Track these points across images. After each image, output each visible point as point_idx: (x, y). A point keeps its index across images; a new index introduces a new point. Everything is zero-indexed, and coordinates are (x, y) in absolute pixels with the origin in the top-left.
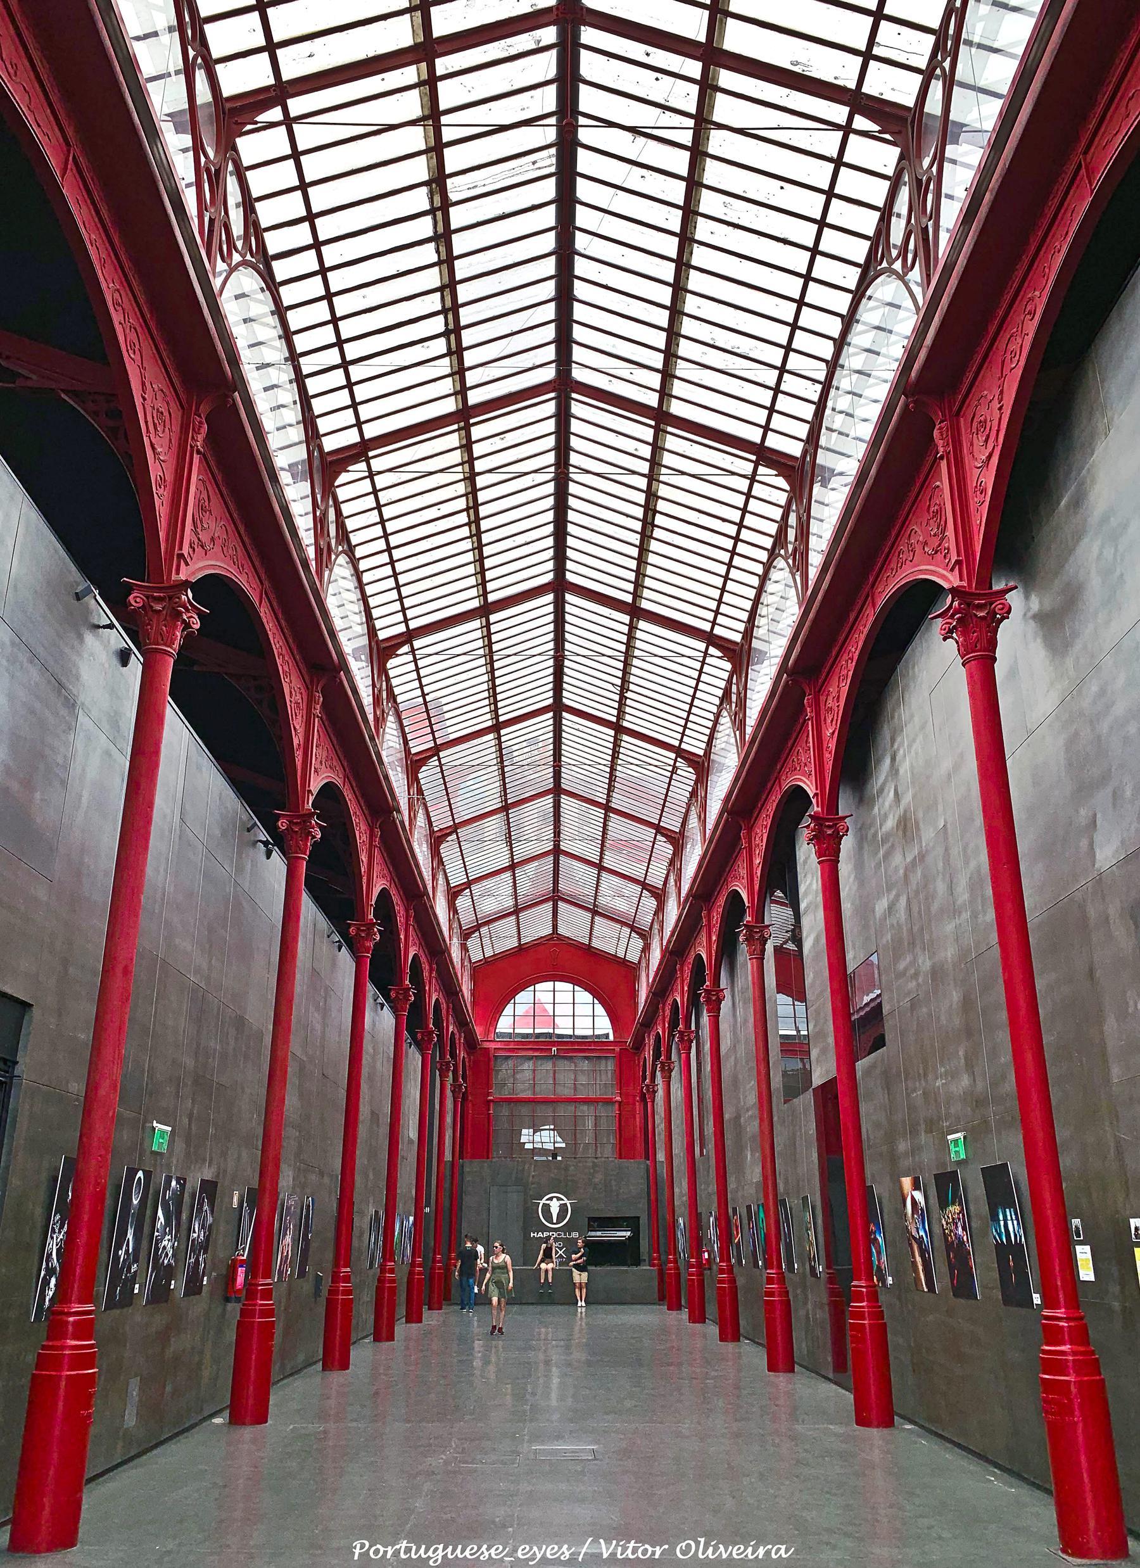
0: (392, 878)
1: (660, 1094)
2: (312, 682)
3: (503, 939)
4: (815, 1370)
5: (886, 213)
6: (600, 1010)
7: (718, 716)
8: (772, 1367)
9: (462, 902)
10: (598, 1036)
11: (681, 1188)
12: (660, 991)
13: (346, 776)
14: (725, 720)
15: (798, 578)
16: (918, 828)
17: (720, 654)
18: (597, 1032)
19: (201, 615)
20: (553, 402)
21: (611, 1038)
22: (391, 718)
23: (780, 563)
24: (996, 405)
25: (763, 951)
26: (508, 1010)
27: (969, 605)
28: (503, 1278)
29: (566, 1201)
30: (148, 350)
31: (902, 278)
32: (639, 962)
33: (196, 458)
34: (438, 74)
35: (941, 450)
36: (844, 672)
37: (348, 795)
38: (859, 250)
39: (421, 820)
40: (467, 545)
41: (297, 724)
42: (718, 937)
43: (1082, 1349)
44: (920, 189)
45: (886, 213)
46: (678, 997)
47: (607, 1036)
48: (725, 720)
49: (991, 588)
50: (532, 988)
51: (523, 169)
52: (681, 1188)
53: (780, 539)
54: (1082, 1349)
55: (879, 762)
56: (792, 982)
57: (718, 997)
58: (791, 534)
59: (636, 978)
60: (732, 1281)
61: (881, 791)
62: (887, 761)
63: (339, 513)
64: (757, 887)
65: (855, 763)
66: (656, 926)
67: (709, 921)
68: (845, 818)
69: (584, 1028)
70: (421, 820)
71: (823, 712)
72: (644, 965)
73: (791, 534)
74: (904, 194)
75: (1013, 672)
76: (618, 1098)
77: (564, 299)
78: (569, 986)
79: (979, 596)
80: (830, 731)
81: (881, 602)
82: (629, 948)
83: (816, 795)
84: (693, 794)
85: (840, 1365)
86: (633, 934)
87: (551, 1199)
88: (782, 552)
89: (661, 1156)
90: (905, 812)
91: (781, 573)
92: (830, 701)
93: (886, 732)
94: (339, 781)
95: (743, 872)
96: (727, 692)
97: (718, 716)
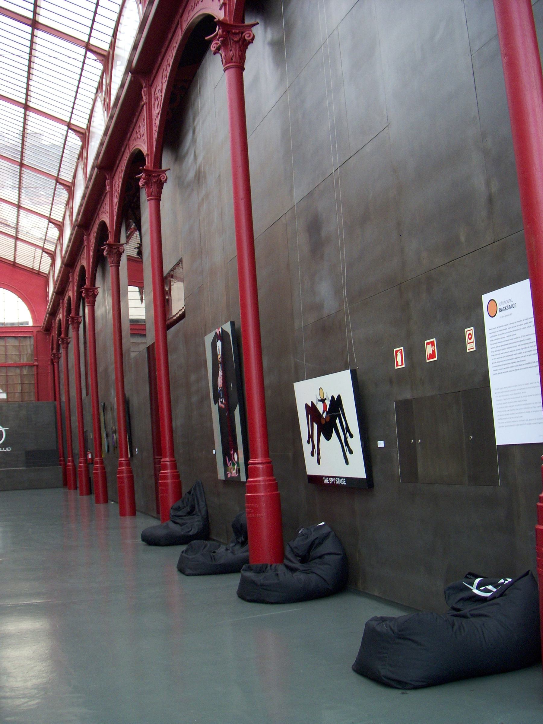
1: (62, 361)
4: (146, 513)
7: (95, 101)
8: (122, 513)
11: (75, 418)
12: (60, 292)
16: (205, 177)
17: (95, 58)
25: (119, 261)
27: (228, 32)
36: (165, 73)
42: (94, 253)
43: (271, 478)
46: (71, 293)
47: (27, 323)
49: (243, 22)
52: (75, 418)
54: (271, 478)
55: (186, 134)
56: (136, 280)
57: (119, 251)
59: (47, 284)
61: (187, 153)
65: (174, 131)
67: (88, 243)
68: (123, 244)
71: (153, 100)
72: (51, 274)
75: (256, 79)
76: (36, 363)
80: (157, 111)
81: (185, 26)
82: (44, 265)
85: (158, 513)
86: (44, 254)
89: (64, 398)
90: (200, 166)
93: (191, 114)
95: (107, 208)
96: (100, 84)
97: (95, 101)
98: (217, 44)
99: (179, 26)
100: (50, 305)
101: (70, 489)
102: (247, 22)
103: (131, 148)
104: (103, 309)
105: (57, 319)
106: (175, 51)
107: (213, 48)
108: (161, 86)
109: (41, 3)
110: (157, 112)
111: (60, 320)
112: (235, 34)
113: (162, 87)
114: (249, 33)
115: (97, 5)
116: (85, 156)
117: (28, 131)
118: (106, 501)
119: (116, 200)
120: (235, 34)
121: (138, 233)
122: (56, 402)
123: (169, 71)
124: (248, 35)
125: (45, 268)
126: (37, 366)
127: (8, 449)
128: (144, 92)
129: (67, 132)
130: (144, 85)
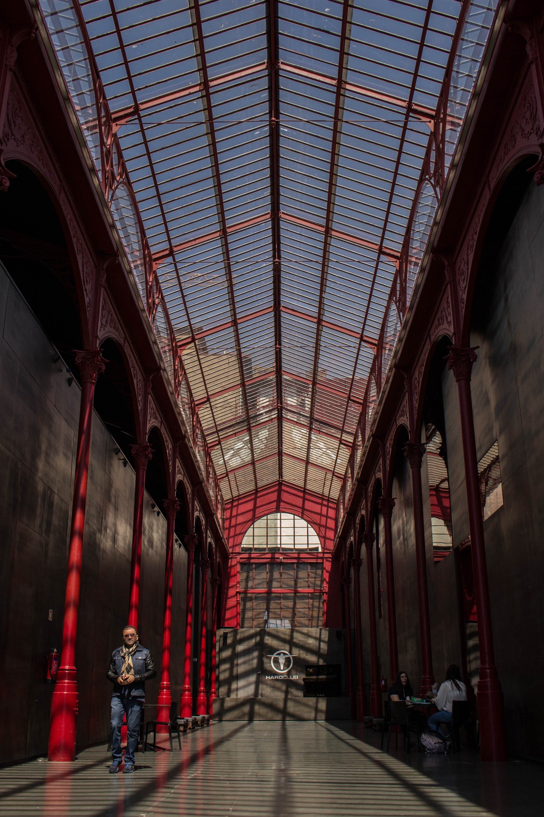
6: (312, 531)
7: (388, 308)
10: (311, 549)
14: (394, 307)
18: (310, 546)
19: (10, 179)
21: (320, 550)
22: (160, 309)
26: (250, 532)
29: (289, 655)
32: (339, 499)
33: (9, 75)
34: (200, 57)
35: (531, 57)
36: (471, 242)
37: (128, 351)
39: (184, 393)
41: (88, 287)
42: (390, 462)
43: (250, 735)
48: (394, 307)
50: (265, 518)
51: (255, 99)
53: (425, 170)
54: (250, 735)
58: (432, 166)
60: (408, 679)
62: (502, 303)
63: (120, 156)
64: (415, 417)
69: (301, 543)
70: (184, 393)
73: (432, 166)
78: (291, 516)
80: (463, 285)
84: (373, 370)
87: (279, 654)
88: (427, 177)
91: (428, 191)
97: (388, 308)
98: (540, 173)
99: (487, 185)
100: (340, 528)
103: (433, 338)
105: (349, 542)
106: (482, 214)
107: (536, 178)
108: (467, 258)
110: (464, 286)
111: (351, 542)
113: (468, 259)
115: (429, 11)
119: (416, 397)
123: (476, 239)
125: (335, 494)
130: (446, 263)
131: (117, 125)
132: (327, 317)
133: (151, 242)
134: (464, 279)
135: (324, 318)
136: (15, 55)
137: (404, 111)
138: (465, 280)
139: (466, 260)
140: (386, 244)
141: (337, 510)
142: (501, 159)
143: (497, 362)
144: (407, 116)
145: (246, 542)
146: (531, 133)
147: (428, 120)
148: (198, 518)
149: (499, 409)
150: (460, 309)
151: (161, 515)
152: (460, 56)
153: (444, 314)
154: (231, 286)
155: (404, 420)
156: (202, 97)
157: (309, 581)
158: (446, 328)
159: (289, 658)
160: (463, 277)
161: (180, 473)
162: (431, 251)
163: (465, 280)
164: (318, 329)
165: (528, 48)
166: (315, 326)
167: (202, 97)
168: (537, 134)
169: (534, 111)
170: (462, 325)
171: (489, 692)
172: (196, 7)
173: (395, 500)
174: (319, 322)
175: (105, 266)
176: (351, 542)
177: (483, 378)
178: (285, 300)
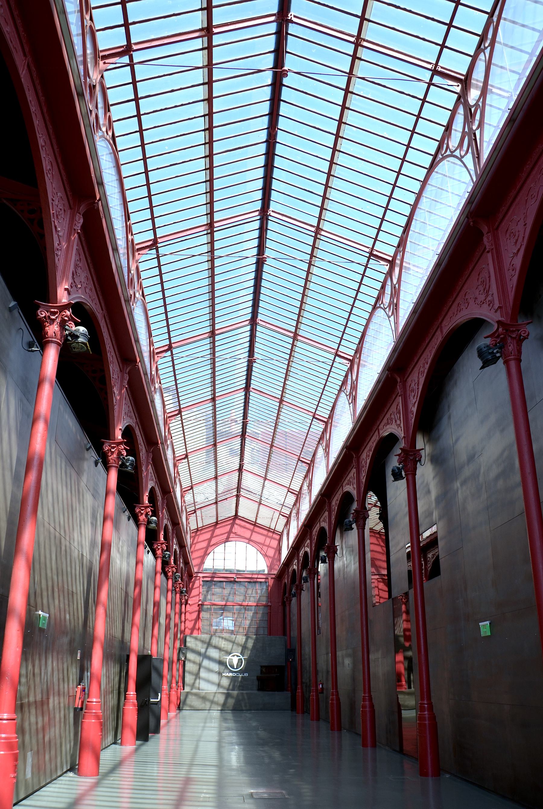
0: (156, 482)
2: (123, 368)
3: (208, 517)
5: (448, 128)
9: (192, 518)
13: (137, 423)
15: (352, 407)
20: (258, 221)
23: (343, 395)
24: (521, 223)
27: (507, 330)
28: (373, 570)
29: (241, 657)
30: (56, 171)
31: (460, 158)
32: (283, 531)
36: (422, 369)
38: (432, 147)
40: (207, 297)
44: (469, 116)
45: (448, 128)
47: (264, 571)
66: (305, 487)
71: (408, 392)
74: (460, 119)
77: (269, 167)
79: (411, 452)
81: (446, 331)
83: (404, 437)
87: (234, 656)
92: (413, 385)
94: (134, 425)
101: (298, 713)
102: (520, 322)
104: (341, 563)
109: (376, 11)
110: (414, 401)
112: (513, 331)
113: (418, 381)
114: (525, 331)
116: (328, 438)
117: (280, 420)
118: (340, 729)
120: (513, 331)
121: (219, 492)
122: (286, 637)
124: (524, 332)
126: (270, 606)
127: (246, 675)
128: (399, 386)
129: (312, 420)
130: (399, 380)
131: (139, 254)
132: (287, 397)
133: (155, 339)
134: (414, 396)
135: (285, 399)
136: (82, 221)
137: (368, 255)
138: (415, 397)
139: (416, 381)
140: (341, 349)
141: (280, 540)
142: (454, 313)
143: (437, 460)
144: (369, 258)
145: (208, 564)
146: (483, 303)
147: (386, 264)
148: (175, 549)
149: (438, 500)
150: (410, 418)
151: (150, 553)
152: (416, 220)
153: (393, 416)
154: (214, 372)
155: (350, 488)
156: (207, 234)
157: (255, 595)
158: (393, 427)
159: (241, 659)
160: (413, 394)
161: (152, 480)
162: (387, 370)
163: (415, 397)
164: (279, 407)
165: (485, 240)
166: (278, 404)
167: (207, 234)
168: (489, 305)
169: (487, 287)
170: (411, 431)
171: (427, 722)
172: (209, 9)
173: (338, 547)
174: (281, 401)
175: (127, 371)
176: (294, 570)
177: (425, 473)
178: (254, 383)
